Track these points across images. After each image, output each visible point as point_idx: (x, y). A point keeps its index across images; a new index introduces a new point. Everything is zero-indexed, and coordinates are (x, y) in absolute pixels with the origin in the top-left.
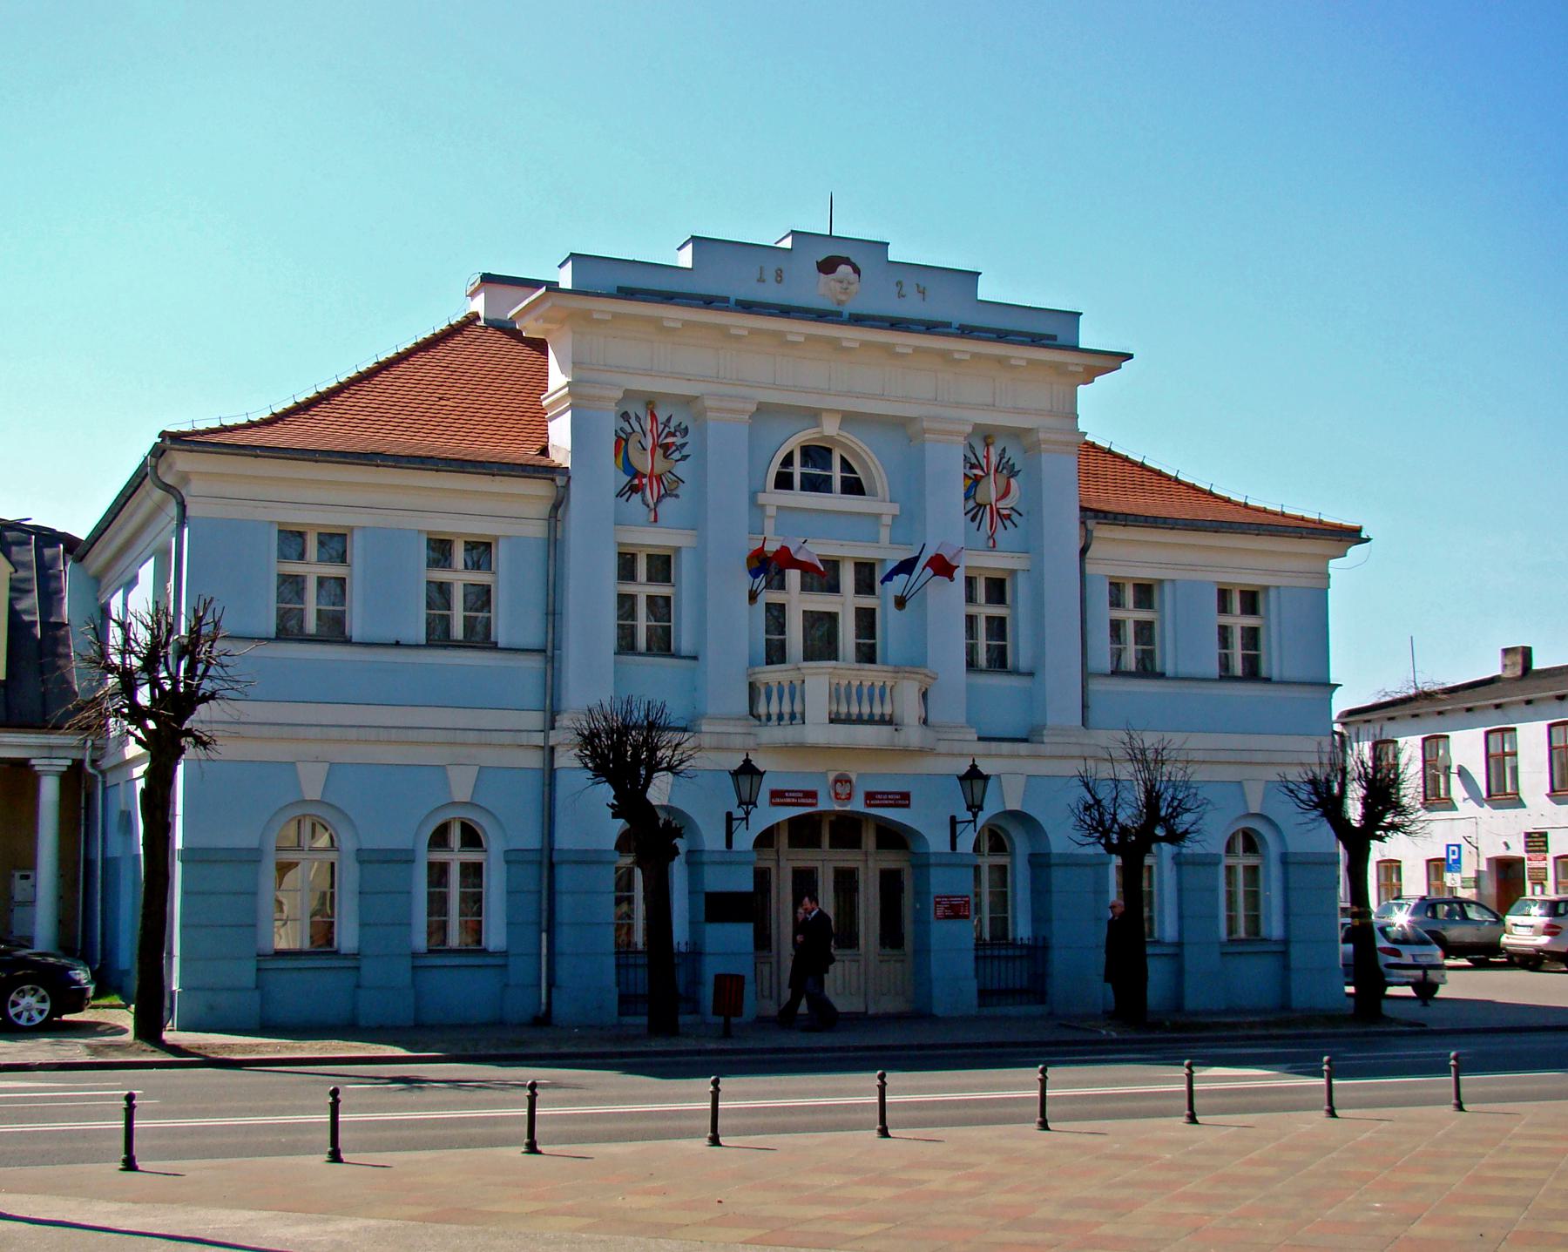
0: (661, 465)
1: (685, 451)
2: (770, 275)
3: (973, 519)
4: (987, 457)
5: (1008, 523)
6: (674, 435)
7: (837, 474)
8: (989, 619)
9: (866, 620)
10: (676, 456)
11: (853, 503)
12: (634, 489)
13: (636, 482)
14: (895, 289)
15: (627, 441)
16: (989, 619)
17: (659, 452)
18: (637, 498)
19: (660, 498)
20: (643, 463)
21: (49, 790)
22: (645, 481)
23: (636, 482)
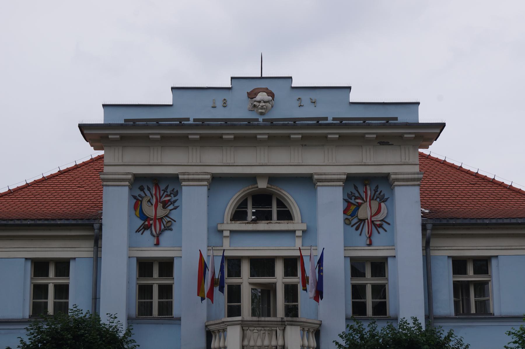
0: (161, 212)
1: (176, 204)
2: (219, 104)
3: (357, 229)
4: (366, 192)
5: (380, 230)
6: (169, 196)
7: (275, 209)
8: (374, 287)
9: (291, 292)
10: (171, 207)
11: (284, 226)
12: (146, 228)
13: (147, 223)
14: (298, 103)
15: (141, 201)
16: (374, 287)
17: (160, 205)
18: (147, 233)
19: (161, 232)
20: (149, 211)
21: (256, 186)
22: (151, 222)
23: (147, 223)
